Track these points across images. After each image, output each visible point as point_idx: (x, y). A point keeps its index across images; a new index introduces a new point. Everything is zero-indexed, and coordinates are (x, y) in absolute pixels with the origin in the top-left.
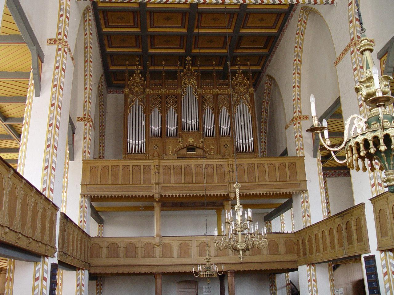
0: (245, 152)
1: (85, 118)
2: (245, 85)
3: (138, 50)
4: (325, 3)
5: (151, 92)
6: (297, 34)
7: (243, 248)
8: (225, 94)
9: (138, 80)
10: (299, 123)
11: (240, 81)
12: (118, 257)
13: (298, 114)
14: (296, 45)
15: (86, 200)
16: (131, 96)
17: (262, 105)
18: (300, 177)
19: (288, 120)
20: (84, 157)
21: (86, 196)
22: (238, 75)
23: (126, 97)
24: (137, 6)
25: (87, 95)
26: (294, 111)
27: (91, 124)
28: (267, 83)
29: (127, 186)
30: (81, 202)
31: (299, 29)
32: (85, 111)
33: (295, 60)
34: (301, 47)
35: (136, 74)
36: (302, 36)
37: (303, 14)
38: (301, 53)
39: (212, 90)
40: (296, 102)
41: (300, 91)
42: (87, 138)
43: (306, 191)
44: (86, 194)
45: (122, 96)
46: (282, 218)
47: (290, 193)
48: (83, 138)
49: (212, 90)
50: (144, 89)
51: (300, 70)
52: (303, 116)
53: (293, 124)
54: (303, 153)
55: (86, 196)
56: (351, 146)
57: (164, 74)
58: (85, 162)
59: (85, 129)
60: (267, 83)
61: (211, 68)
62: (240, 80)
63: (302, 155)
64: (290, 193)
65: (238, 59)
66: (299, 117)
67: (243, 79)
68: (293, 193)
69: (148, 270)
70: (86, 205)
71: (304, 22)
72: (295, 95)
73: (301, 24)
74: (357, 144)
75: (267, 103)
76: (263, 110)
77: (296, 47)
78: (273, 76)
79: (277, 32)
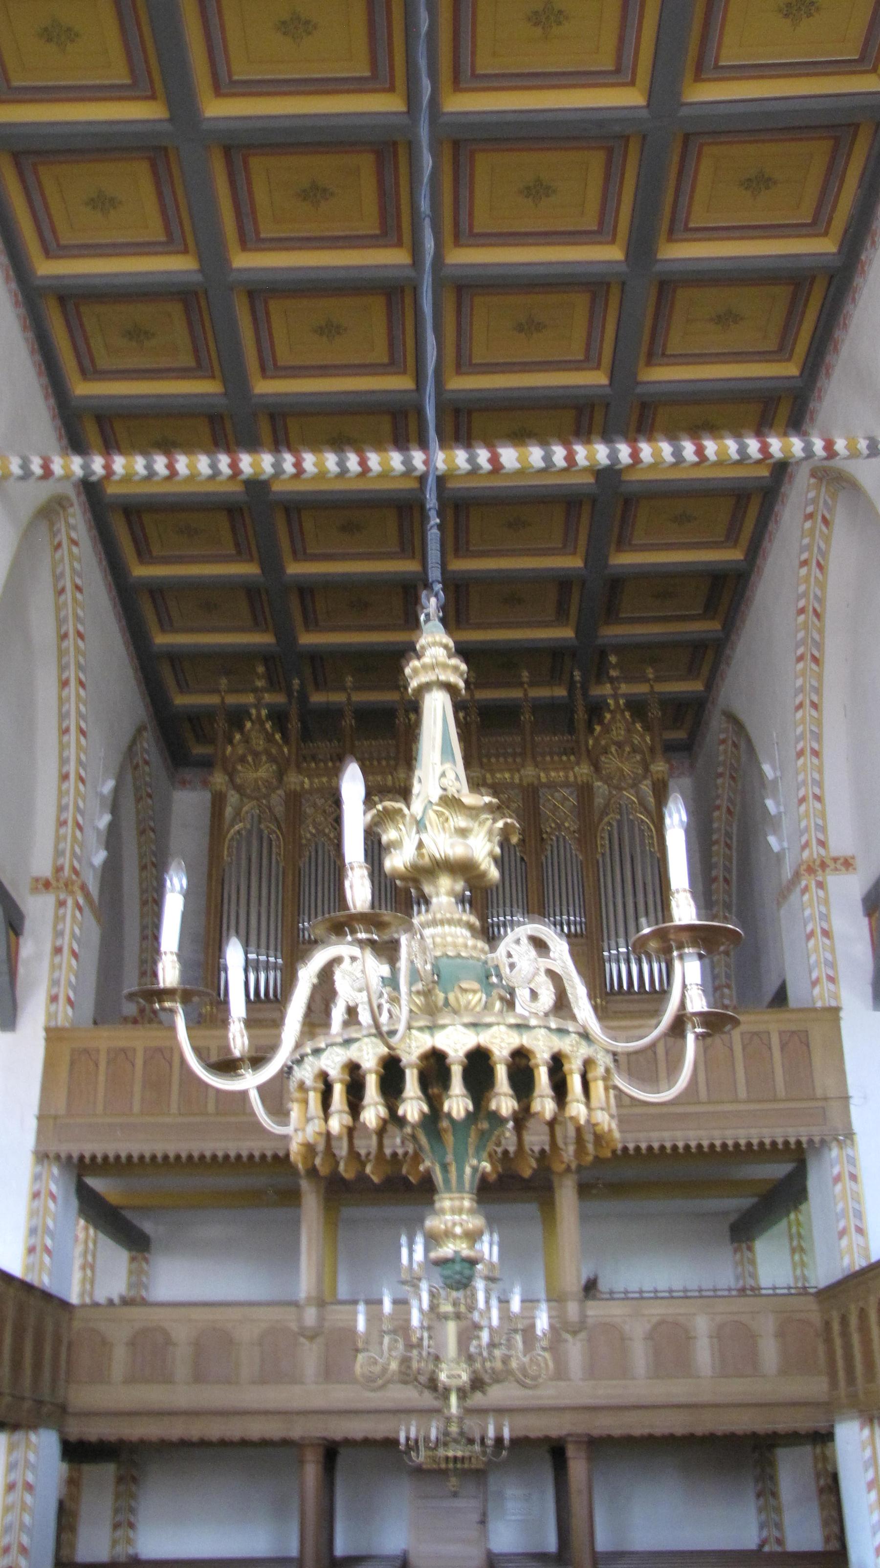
0: (639, 993)
1: (58, 880)
2: (635, 750)
3: (262, 639)
4: (865, 452)
5: (303, 783)
6: (805, 563)
7: (459, 1383)
8: (566, 784)
9: (259, 743)
10: (821, 885)
11: (621, 738)
12: (167, 1379)
13: (816, 850)
14: (801, 604)
15: (55, 1171)
16: (233, 798)
17: (711, 821)
18: (824, 1083)
19: (788, 872)
20: (50, 1016)
21: (51, 1155)
22: (613, 718)
23: (218, 802)
24: (591, 480)
25: (70, 800)
26: (803, 840)
27: (81, 901)
28: (723, 742)
29: (198, 1119)
30: (37, 1177)
31: (808, 548)
32: (58, 853)
33: (800, 658)
34: (819, 610)
35: (253, 722)
36: (818, 570)
37: (818, 494)
38: (821, 632)
39: (518, 771)
40: (807, 811)
41: (820, 771)
42: (66, 951)
43: (850, 1135)
44: (54, 1148)
45: (206, 796)
46: (794, 1230)
47: (799, 1143)
48: (48, 948)
49: (518, 771)
50: (281, 774)
51: (818, 691)
52: (835, 860)
53: (798, 890)
54: (836, 997)
55: (51, 1155)
56: (324, 1077)
57: (348, 722)
58: (54, 1035)
59: (58, 919)
60: (723, 742)
61: (516, 694)
62: (619, 732)
63: (833, 1004)
64: (799, 1143)
65: (613, 659)
66: (818, 862)
67: (629, 731)
68: (811, 1142)
69: (273, 1430)
70: (54, 1188)
71: (825, 521)
72: (804, 783)
73: (812, 530)
74: (353, 1069)
75: (729, 812)
76: (715, 837)
77: (802, 611)
78: (743, 717)
79: (741, 557)
